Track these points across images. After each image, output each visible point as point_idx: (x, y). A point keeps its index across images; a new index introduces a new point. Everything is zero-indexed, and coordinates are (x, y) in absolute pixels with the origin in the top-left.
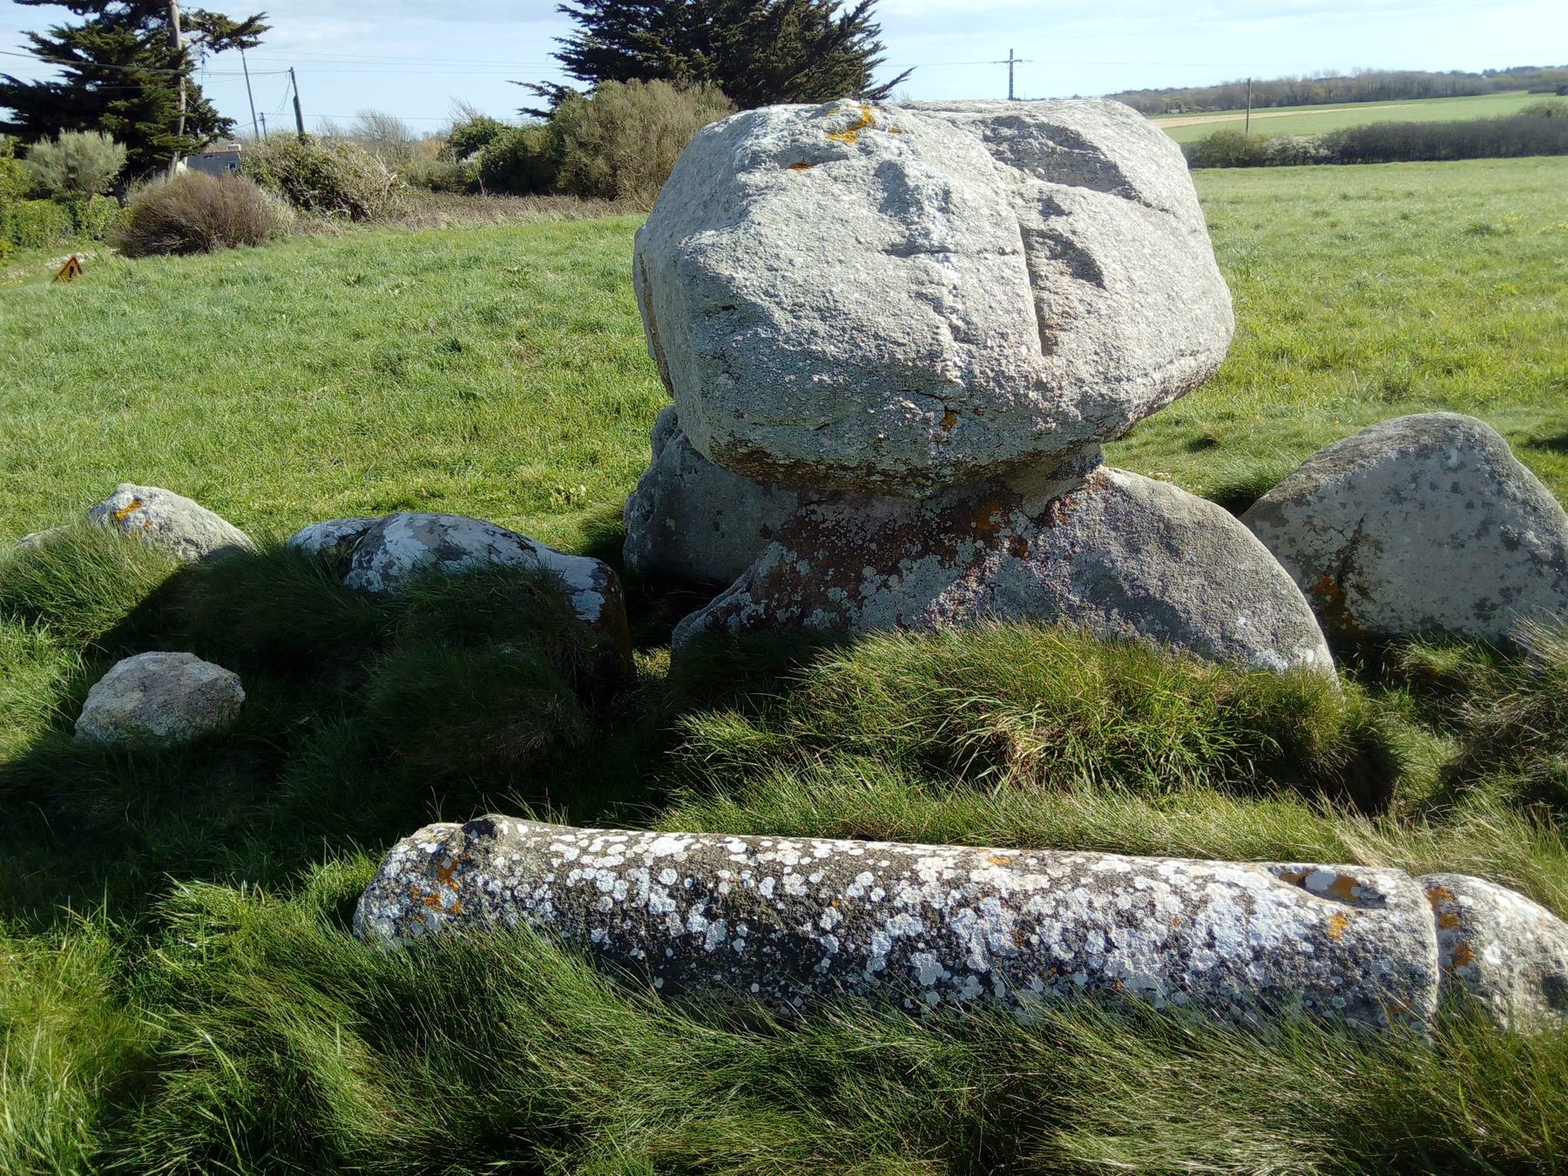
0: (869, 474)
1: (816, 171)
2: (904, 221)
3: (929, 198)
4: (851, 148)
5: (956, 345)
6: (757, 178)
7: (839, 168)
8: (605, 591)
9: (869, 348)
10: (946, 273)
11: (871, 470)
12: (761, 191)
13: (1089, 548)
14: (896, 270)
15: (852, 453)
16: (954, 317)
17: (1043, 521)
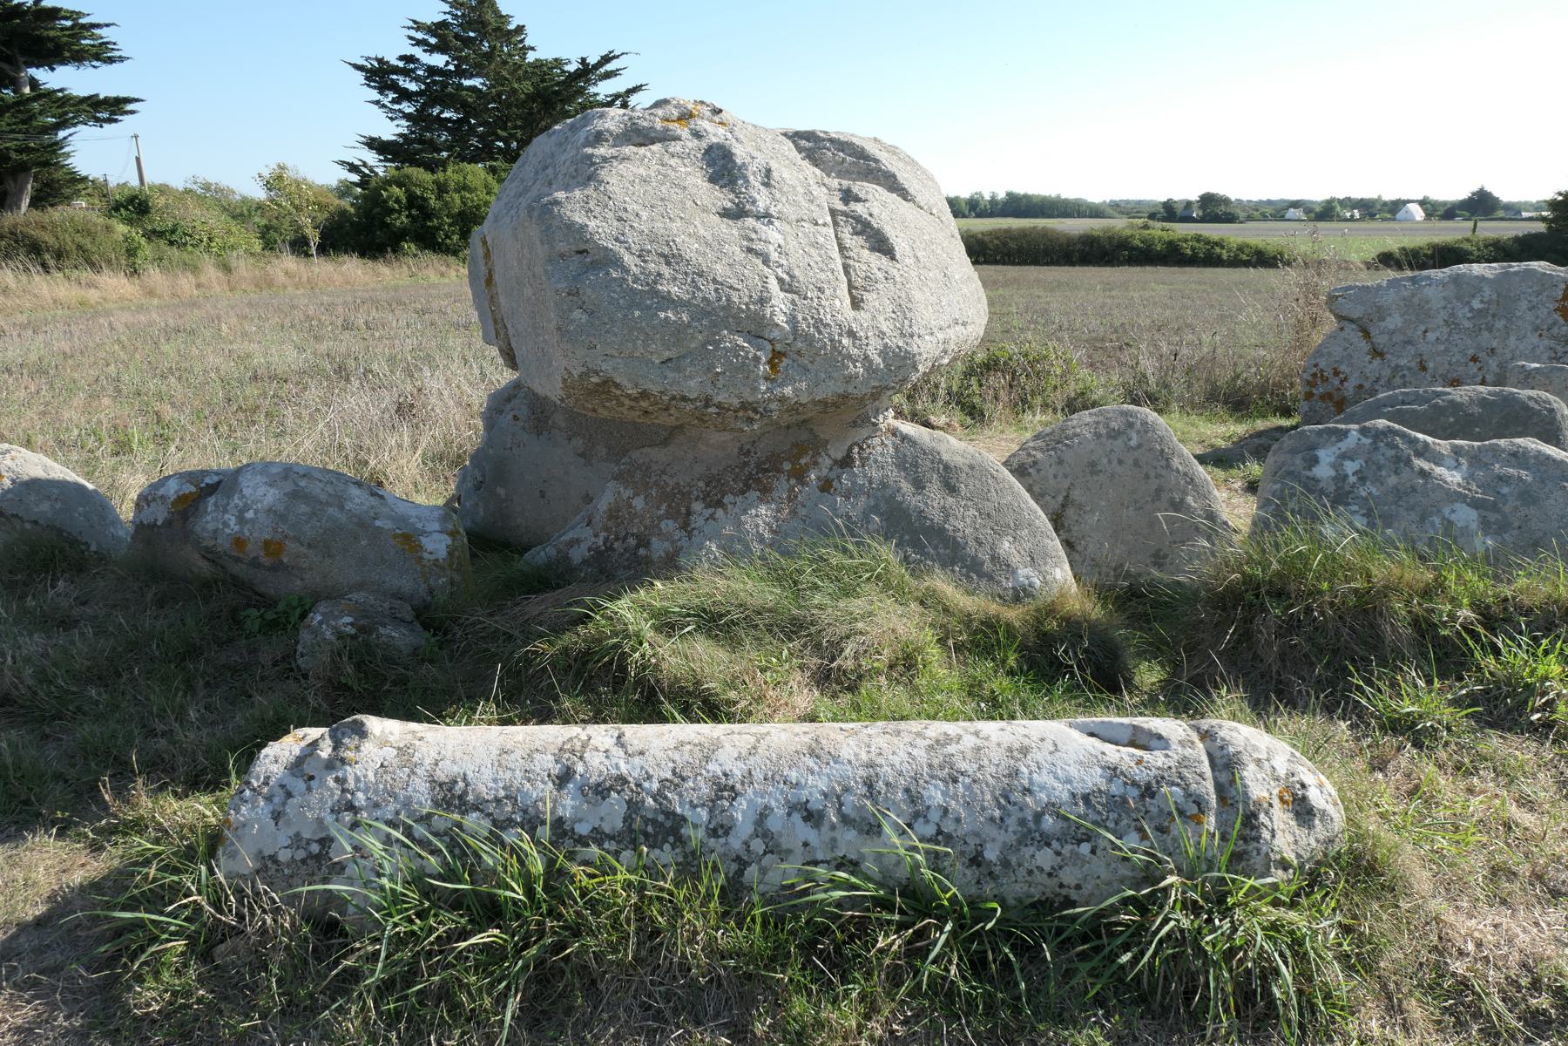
0: (707, 406)
1: (656, 147)
2: (733, 191)
3: (754, 174)
4: (684, 133)
5: (782, 295)
6: (602, 151)
7: (676, 147)
8: (453, 534)
9: (709, 290)
10: (772, 235)
11: (708, 402)
12: (605, 159)
13: (884, 485)
14: (729, 230)
15: (693, 386)
16: (779, 271)
17: (846, 462)
